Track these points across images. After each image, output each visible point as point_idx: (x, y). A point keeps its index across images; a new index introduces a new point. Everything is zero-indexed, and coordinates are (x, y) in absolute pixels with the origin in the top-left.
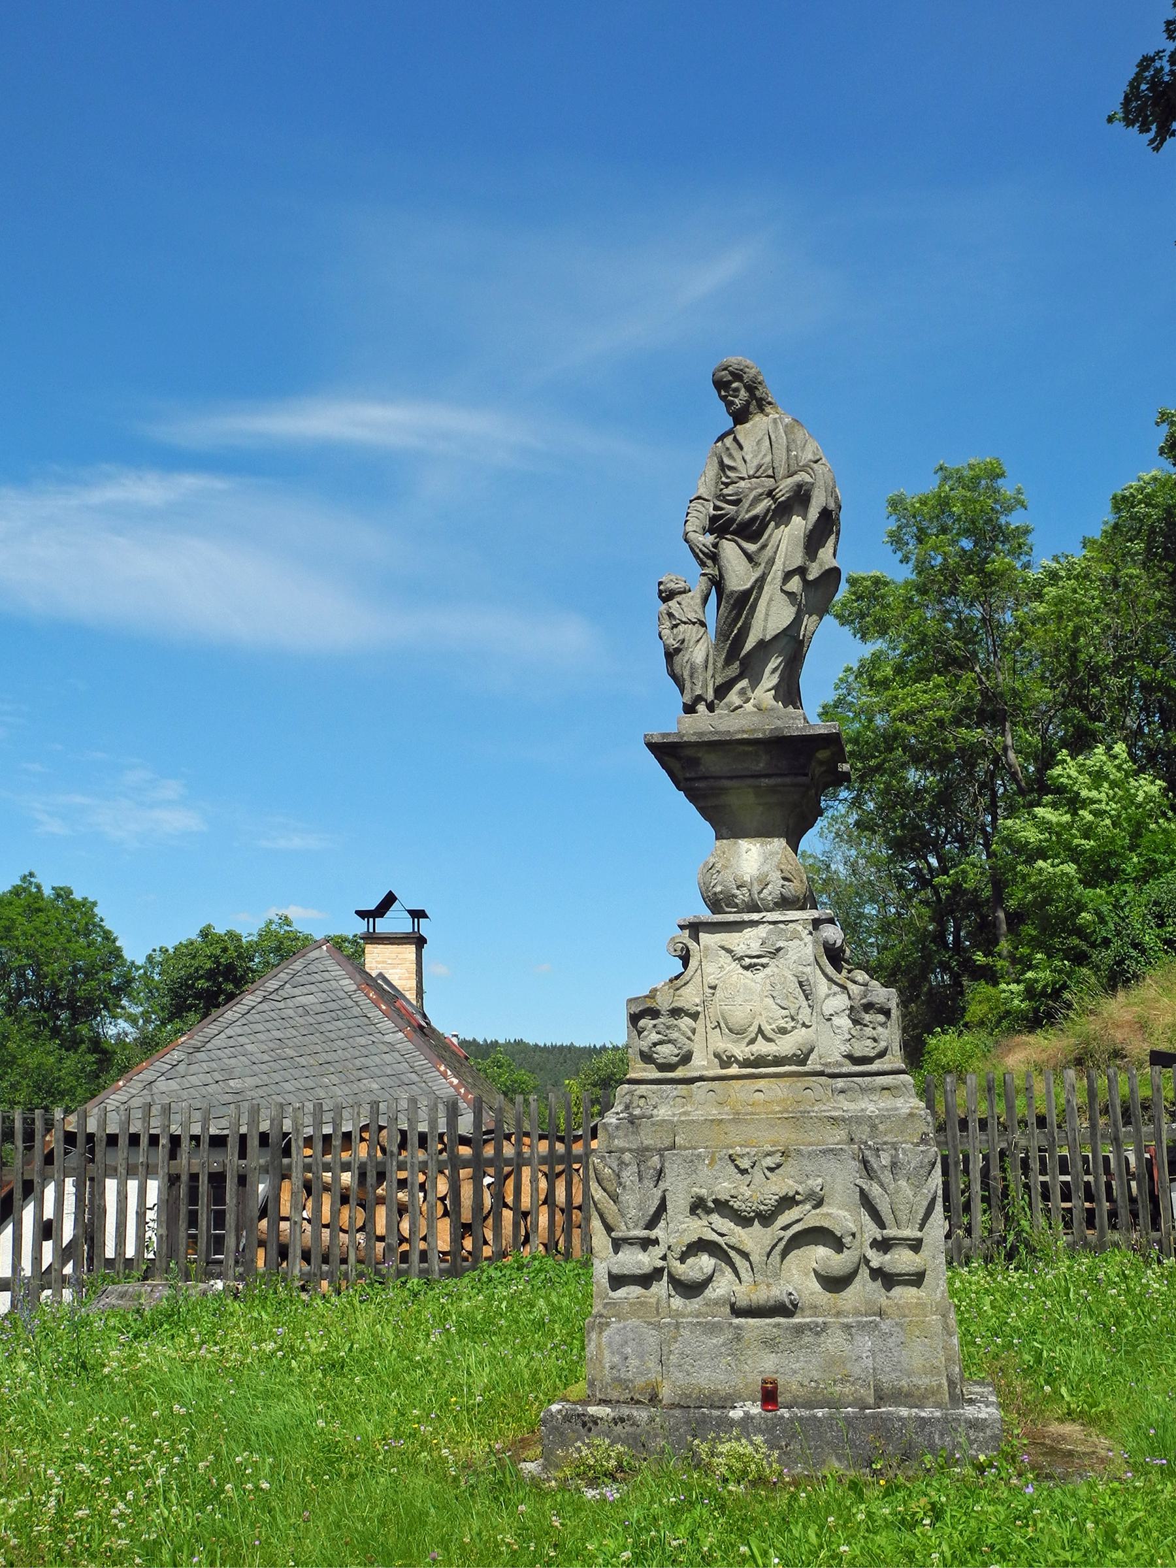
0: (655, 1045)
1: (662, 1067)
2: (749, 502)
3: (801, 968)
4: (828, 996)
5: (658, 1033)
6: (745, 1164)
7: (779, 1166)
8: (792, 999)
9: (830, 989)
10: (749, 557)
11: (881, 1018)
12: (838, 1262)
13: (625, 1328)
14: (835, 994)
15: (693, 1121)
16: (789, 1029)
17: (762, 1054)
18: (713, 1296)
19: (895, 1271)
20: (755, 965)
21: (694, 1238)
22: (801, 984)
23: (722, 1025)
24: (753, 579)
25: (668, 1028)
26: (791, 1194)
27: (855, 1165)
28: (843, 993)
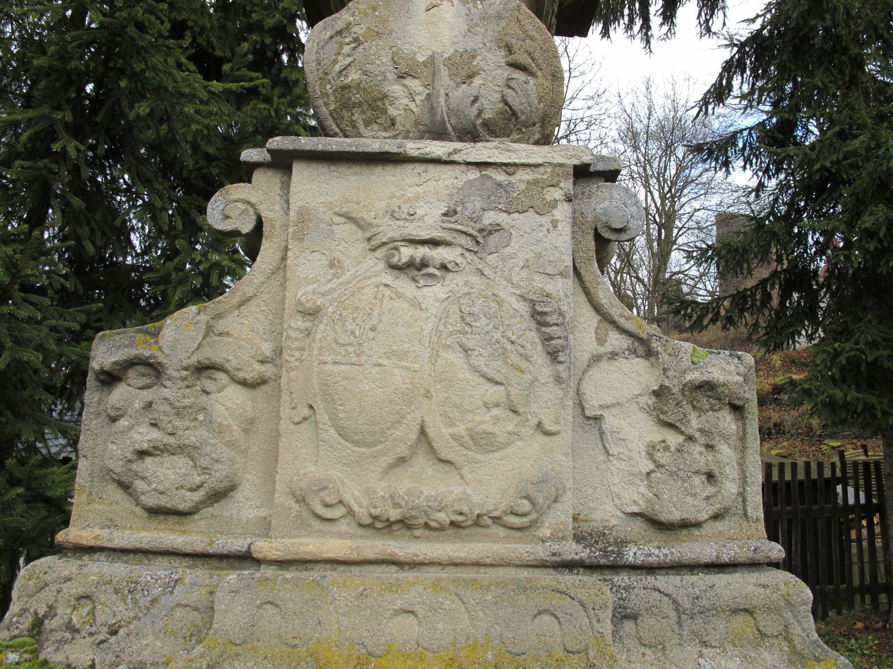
1: (155, 512)
4: (596, 359)
8: (515, 359)
9: (601, 342)
14: (613, 356)
20: (424, 264)
22: (539, 318)
23: (323, 417)
25: (179, 412)
28: (634, 352)
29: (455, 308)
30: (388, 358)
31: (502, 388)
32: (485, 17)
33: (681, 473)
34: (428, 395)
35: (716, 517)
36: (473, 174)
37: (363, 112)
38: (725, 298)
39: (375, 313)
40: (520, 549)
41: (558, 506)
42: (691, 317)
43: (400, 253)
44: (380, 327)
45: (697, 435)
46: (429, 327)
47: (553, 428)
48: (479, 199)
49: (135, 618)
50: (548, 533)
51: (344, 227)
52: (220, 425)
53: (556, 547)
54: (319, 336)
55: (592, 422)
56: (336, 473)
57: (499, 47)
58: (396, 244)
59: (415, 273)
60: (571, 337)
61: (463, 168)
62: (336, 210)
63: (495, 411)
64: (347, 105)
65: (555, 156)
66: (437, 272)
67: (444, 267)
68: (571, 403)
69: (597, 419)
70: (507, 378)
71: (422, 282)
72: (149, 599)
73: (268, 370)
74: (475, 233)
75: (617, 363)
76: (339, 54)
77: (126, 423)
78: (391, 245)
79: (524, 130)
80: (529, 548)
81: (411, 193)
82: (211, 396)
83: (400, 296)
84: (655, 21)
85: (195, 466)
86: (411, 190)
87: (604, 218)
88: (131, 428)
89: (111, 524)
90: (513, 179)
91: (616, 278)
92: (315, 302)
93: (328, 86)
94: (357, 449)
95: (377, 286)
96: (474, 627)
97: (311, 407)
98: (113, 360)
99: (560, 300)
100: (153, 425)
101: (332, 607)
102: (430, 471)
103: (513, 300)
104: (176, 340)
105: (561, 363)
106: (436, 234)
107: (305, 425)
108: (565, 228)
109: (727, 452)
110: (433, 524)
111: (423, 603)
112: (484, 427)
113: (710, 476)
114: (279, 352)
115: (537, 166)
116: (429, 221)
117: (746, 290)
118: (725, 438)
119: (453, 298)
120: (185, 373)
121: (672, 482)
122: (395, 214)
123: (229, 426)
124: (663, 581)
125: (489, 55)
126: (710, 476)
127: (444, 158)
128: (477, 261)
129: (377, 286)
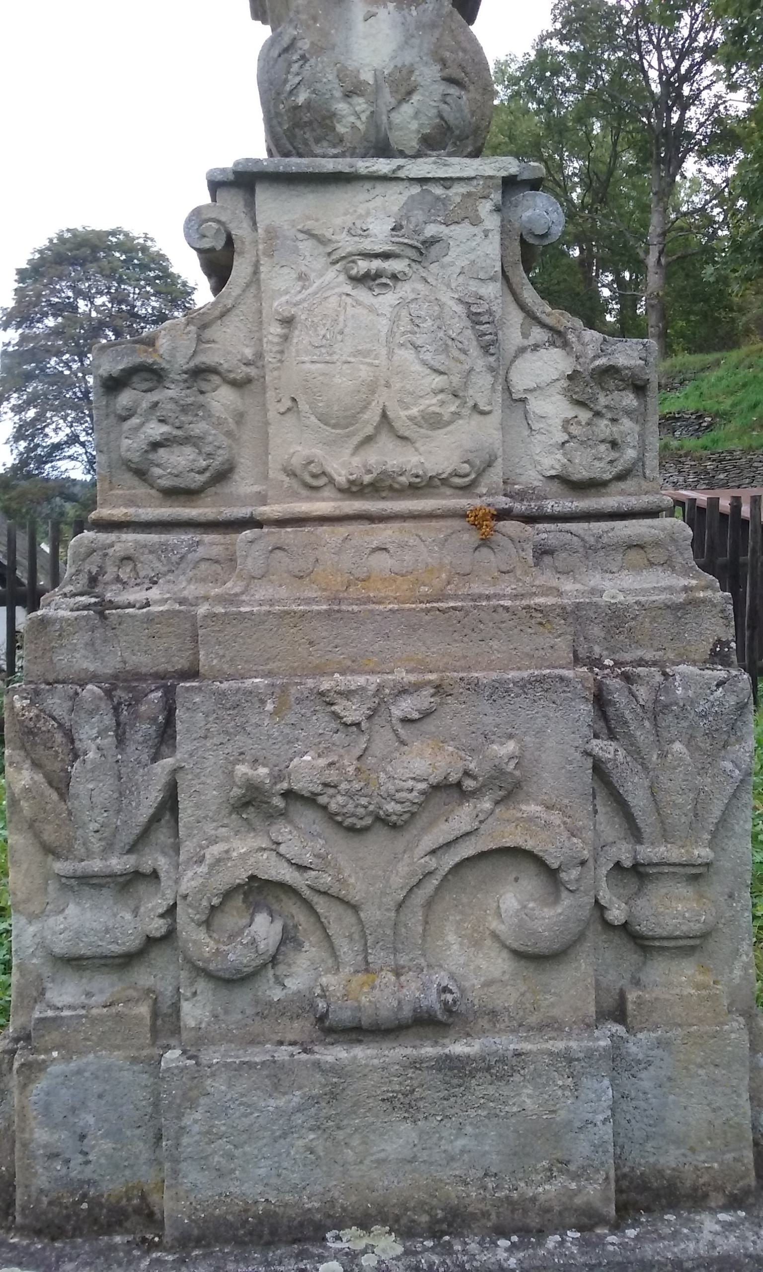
0: (155, 446)
1: (173, 494)
3: (474, 286)
4: (522, 350)
5: (162, 421)
6: (353, 711)
7: (426, 714)
8: (455, 353)
9: (525, 335)
11: (629, 400)
14: (536, 347)
15: (242, 616)
16: (446, 417)
17: (389, 468)
18: (277, 994)
19: (659, 931)
20: (378, 275)
21: (242, 876)
22: (475, 319)
23: (303, 406)
25: (185, 409)
26: (453, 778)
27: (585, 710)
28: (553, 344)
29: (404, 313)
30: (355, 356)
31: (446, 377)
32: (420, 26)
33: (590, 442)
34: (388, 385)
36: (416, 190)
37: (313, 130)
39: (341, 318)
40: (462, 503)
41: (492, 469)
43: (358, 266)
44: (347, 330)
45: (604, 411)
47: (487, 408)
48: (421, 212)
49: (169, 571)
50: (484, 491)
51: (306, 243)
52: (219, 418)
53: (490, 500)
54: (295, 341)
55: (518, 404)
56: (318, 452)
57: (435, 61)
58: (354, 257)
59: (371, 283)
60: (500, 332)
61: (406, 183)
62: (299, 227)
63: (441, 396)
65: (486, 167)
66: (388, 282)
67: (394, 277)
68: (500, 388)
69: (523, 401)
70: (449, 369)
71: (377, 291)
72: (179, 556)
74: (420, 245)
75: (538, 354)
76: (289, 72)
77: (138, 421)
78: (350, 259)
79: (458, 143)
80: (469, 501)
82: (207, 395)
83: (359, 303)
85: (200, 453)
86: (361, 206)
87: (528, 226)
88: (142, 424)
90: (451, 192)
92: (290, 312)
93: (282, 106)
94: (333, 431)
95: (340, 295)
96: (432, 557)
97: (294, 400)
98: (120, 367)
99: (491, 301)
100: (161, 421)
101: (325, 549)
102: (391, 446)
103: (451, 303)
104: (174, 348)
105: (493, 354)
106: (386, 248)
107: (289, 415)
110: (396, 486)
111: (394, 542)
112: (432, 409)
115: (469, 179)
116: (381, 237)
119: (403, 303)
120: (186, 376)
121: (583, 450)
122: (352, 232)
123: (226, 419)
125: (426, 70)
127: (390, 175)
128: (421, 270)
129: (340, 295)
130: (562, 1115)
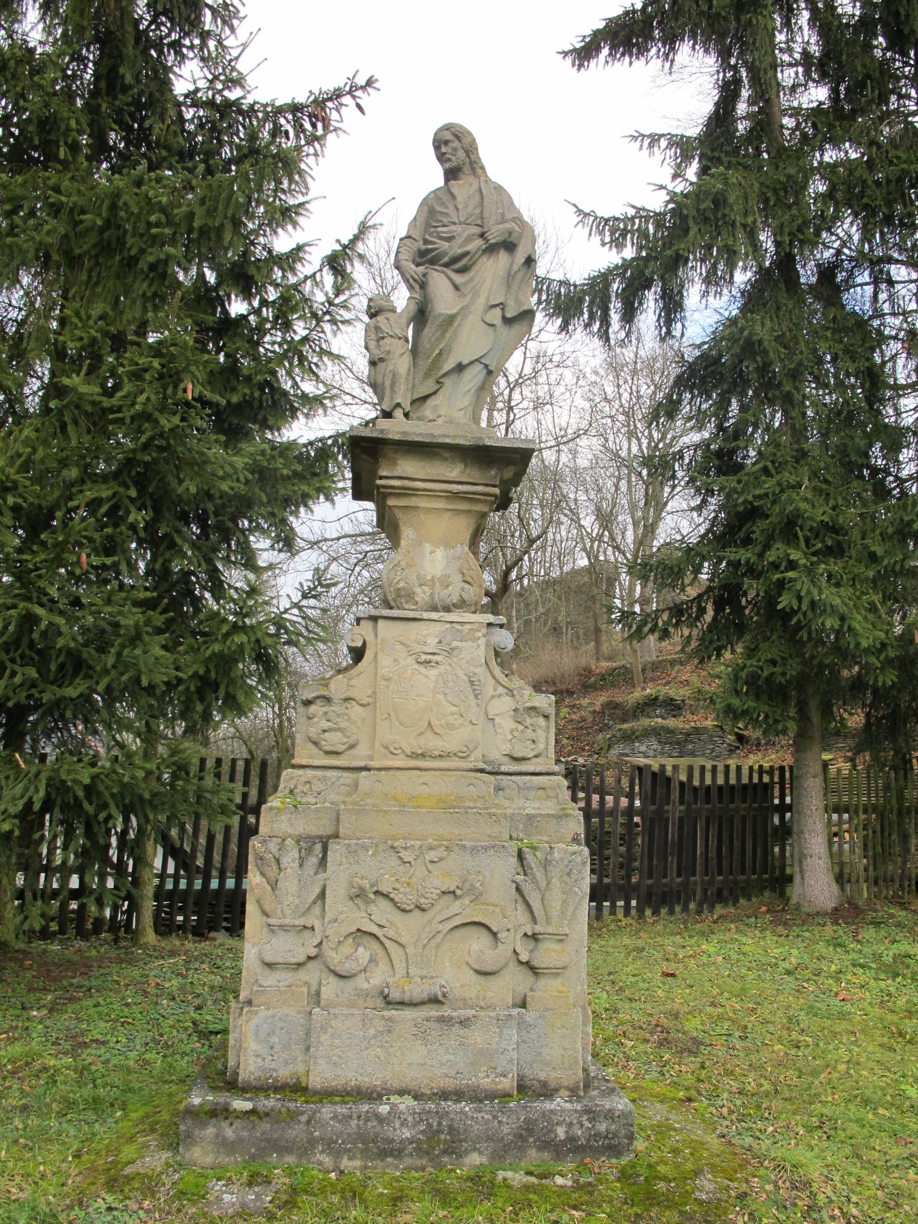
1: (328, 753)
2: (462, 240)
4: (493, 697)
6: (407, 856)
9: (495, 690)
10: (457, 288)
12: (492, 956)
13: (273, 1017)
14: (500, 695)
18: (365, 986)
20: (430, 662)
22: (472, 683)
23: (393, 718)
24: (459, 307)
25: (338, 716)
35: (536, 756)
36: (448, 626)
38: (663, 611)
42: (630, 627)
46: (432, 685)
64: (399, 596)
73: (370, 700)
81: (424, 633)
84: (615, 318)
89: (311, 757)
91: (592, 547)
108: (483, 648)
109: (541, 734)
113: (534, 741)
114: (374, 693)
117: (682, 603)
118: (540, 727)
119: (440, 675)
124: (514, 778)
126: (534, 741)
130: (494, 1046)
